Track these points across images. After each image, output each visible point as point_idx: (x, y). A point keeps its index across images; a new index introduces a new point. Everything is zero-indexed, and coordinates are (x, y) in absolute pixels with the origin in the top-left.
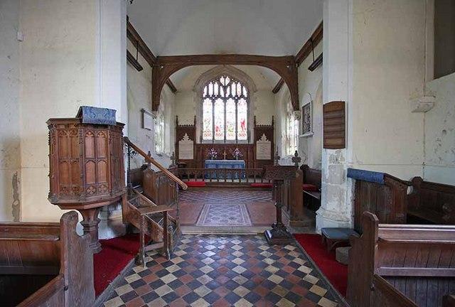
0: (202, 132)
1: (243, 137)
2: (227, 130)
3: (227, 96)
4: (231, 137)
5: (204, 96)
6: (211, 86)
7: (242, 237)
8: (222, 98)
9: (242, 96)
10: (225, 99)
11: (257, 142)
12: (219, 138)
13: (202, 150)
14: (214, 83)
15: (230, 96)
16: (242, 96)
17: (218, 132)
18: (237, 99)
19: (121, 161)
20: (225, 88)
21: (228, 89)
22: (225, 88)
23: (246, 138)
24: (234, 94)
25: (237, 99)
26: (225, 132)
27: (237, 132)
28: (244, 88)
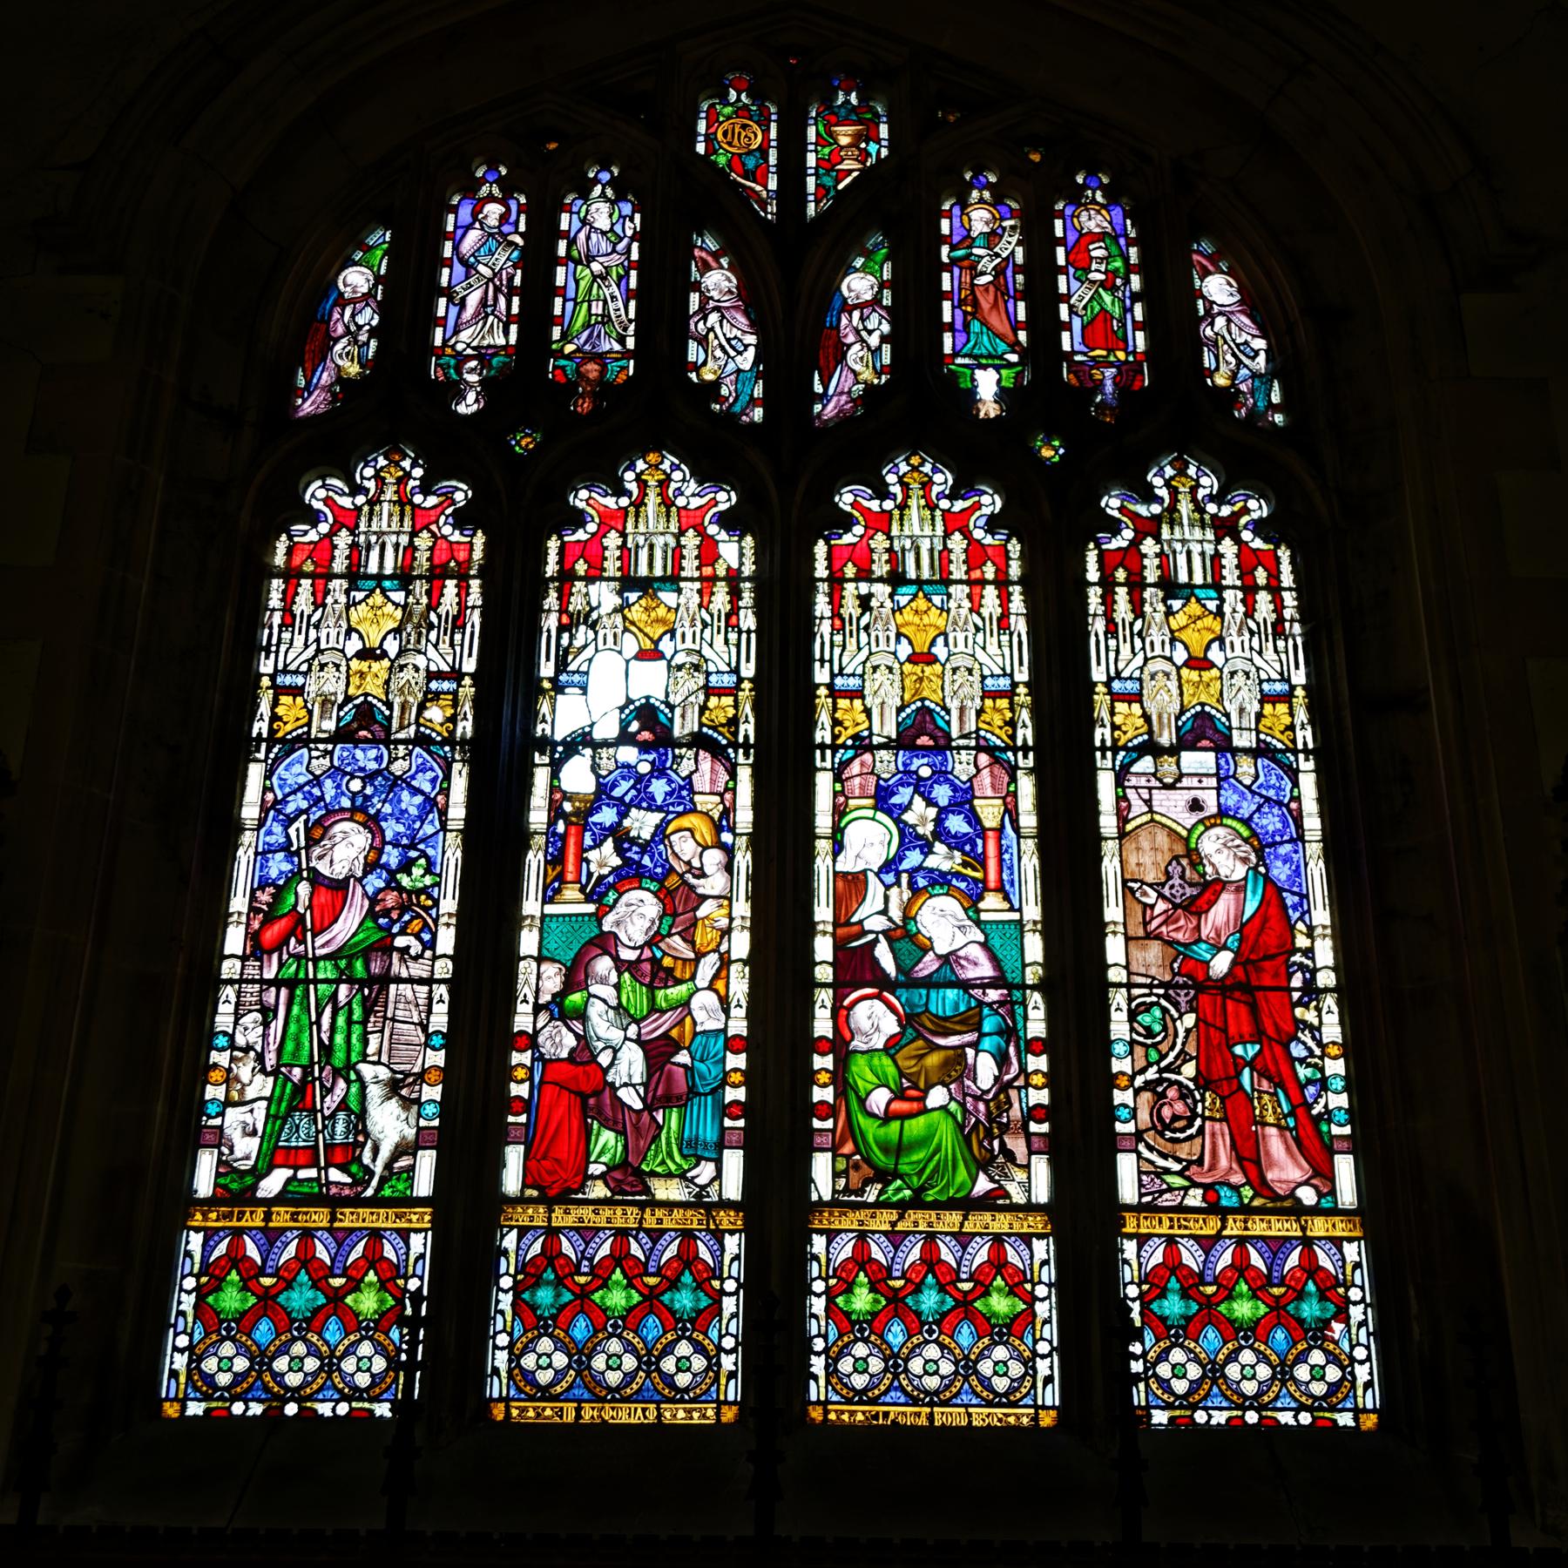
6: (481, 236)
23: (1342, 1375)
26: (777, 1215)
27: (1085, 1219)
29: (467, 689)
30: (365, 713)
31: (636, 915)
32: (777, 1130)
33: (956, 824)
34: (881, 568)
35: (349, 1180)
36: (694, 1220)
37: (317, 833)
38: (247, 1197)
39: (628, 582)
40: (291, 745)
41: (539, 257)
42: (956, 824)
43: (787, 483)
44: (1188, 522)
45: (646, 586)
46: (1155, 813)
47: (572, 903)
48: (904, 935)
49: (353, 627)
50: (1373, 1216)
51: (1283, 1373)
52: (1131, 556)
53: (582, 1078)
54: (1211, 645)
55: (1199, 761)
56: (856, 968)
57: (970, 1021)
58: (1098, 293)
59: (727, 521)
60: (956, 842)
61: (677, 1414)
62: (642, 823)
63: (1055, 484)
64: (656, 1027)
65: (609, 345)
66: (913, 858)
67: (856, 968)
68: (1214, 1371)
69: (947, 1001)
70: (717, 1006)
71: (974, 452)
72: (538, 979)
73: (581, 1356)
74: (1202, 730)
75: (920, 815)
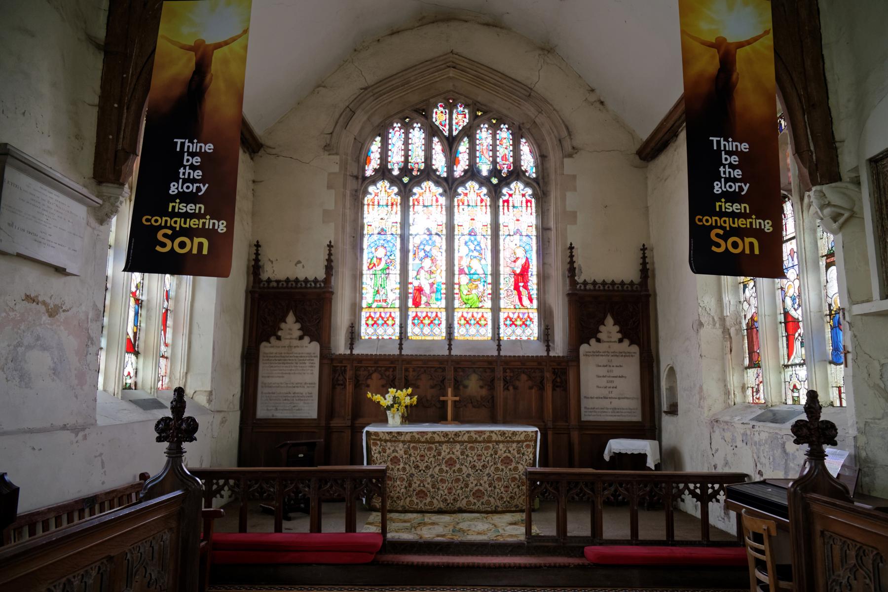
0: (356, 308)
1: (523, 331)
2: (457, 304)
4: (474, 333)
5: (369, 172)
6: (396, 137)
9: (517, 173)
11: (584, 348)
12: (427, 333)
13: (352, 378)
15: (472, 173)
16: (517, 173)
20: (451, 143)
21: (463, 147)
22: (451, 143)
23: (533, 332)
24: (485, 169)
26: (450, 309)
27: (496, 309)
28: (525, 149)
29: (399, 225)
30: (382, 230)
31: (427, 263)
32: (450, 297)
33: (478, 248)
34: (466, 203)
35: (436, 140)
36: (437, 310)
37: (376, 249)
38: (370, 307)
39: (424, 206)
40: (371, 235)
41: (406, 143)
42: (478, 248)
43: (450, 185)
44: (518, 192)
45: (427, 206)
46: (507, 246)
47: (417, 261)
48: (469, 267)
49: (379, 209)
50: (539, 310)
51: (524, 332)
52: (507, 201)
53: (420, 290)
54: (520, 216)
55: (517, 237)
56: (462, 271)
57: (479, 280)
58: (505, 150)
59: (441, 195)
60: (478, 251)
61: (436, 338)
62: (428, 248)
63: (496, 184)
64: (431, 281)
65: (419, 161)
66: (471, 254)
67: (462, 271)
68: (514, 332)
69: (475, 277)
70: (441, 277)
71: (484, 182)
72: (412, 274)
73: (422, 330)
74: (518, 232)
75: (472, 247)
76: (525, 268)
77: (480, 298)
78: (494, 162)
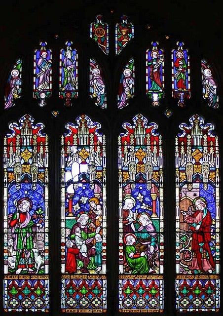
3: (123, 100)
6: (42, 60)
7: (87, 234)
8: (97, 115)
10: (112, 122)
14: (56, 50)
15: (140, 103)
17: (78, 278)
18: (169, 124)
19: (60, 299)
25: (169, 124)
26: (113, 276)
27: (170, 276)
56: (127, 229)
72: (65, 233)
76: (207, 223)
77: (151, 263)
78: (168, 89)
